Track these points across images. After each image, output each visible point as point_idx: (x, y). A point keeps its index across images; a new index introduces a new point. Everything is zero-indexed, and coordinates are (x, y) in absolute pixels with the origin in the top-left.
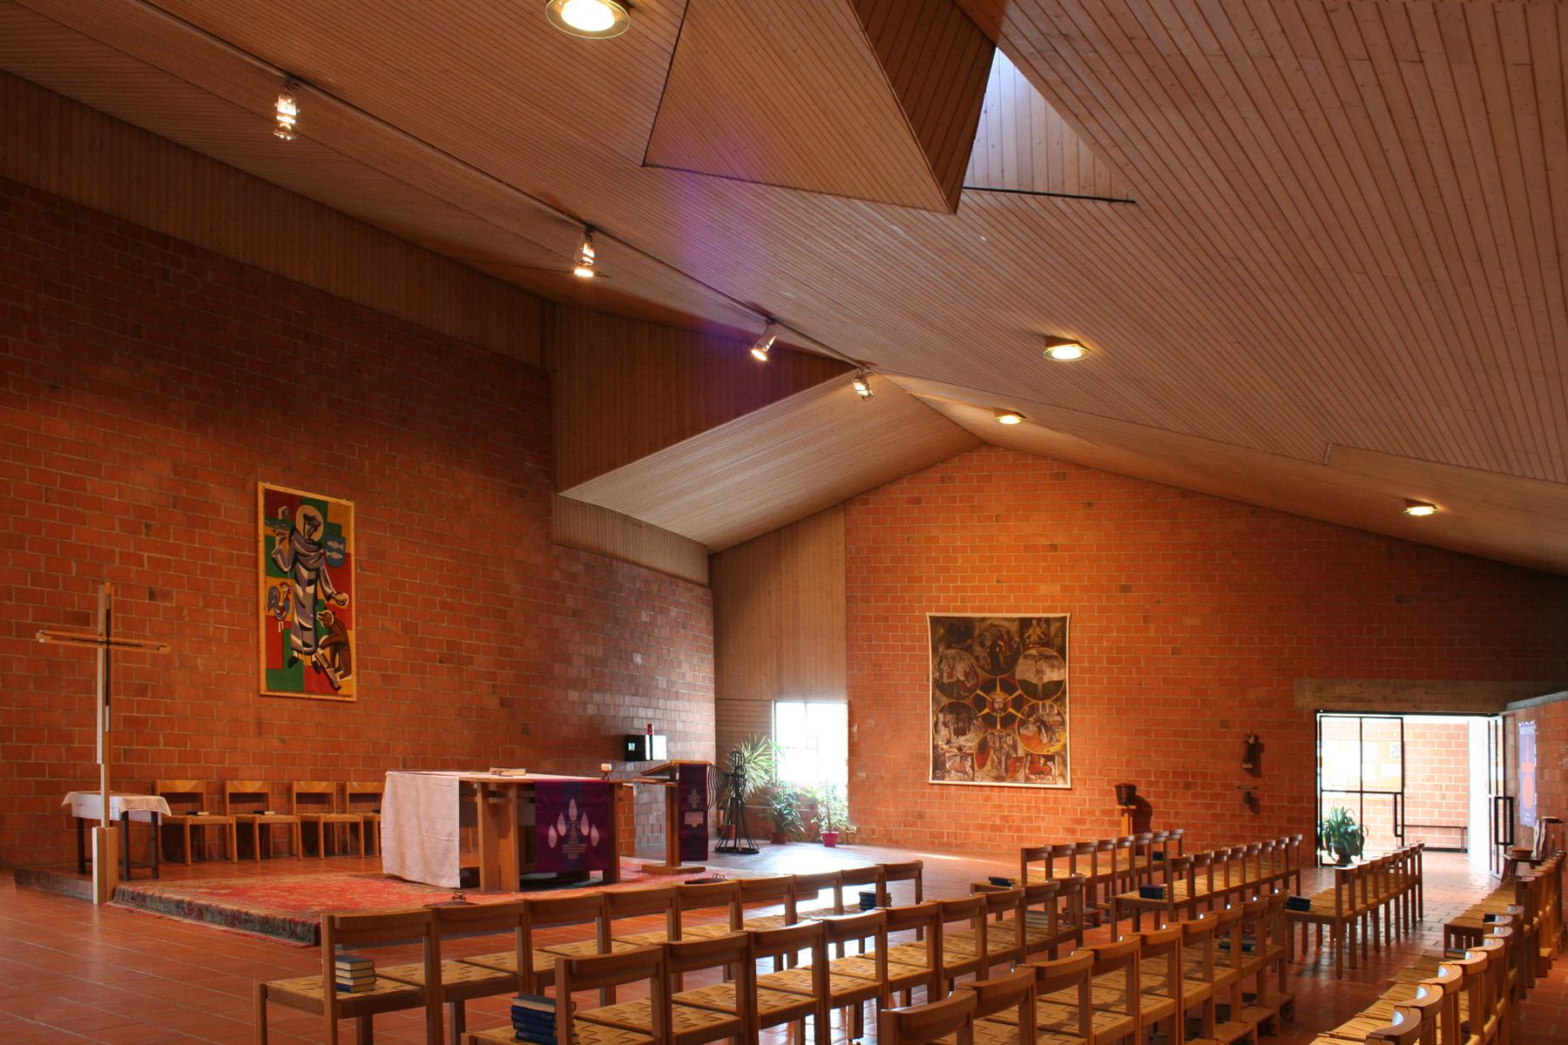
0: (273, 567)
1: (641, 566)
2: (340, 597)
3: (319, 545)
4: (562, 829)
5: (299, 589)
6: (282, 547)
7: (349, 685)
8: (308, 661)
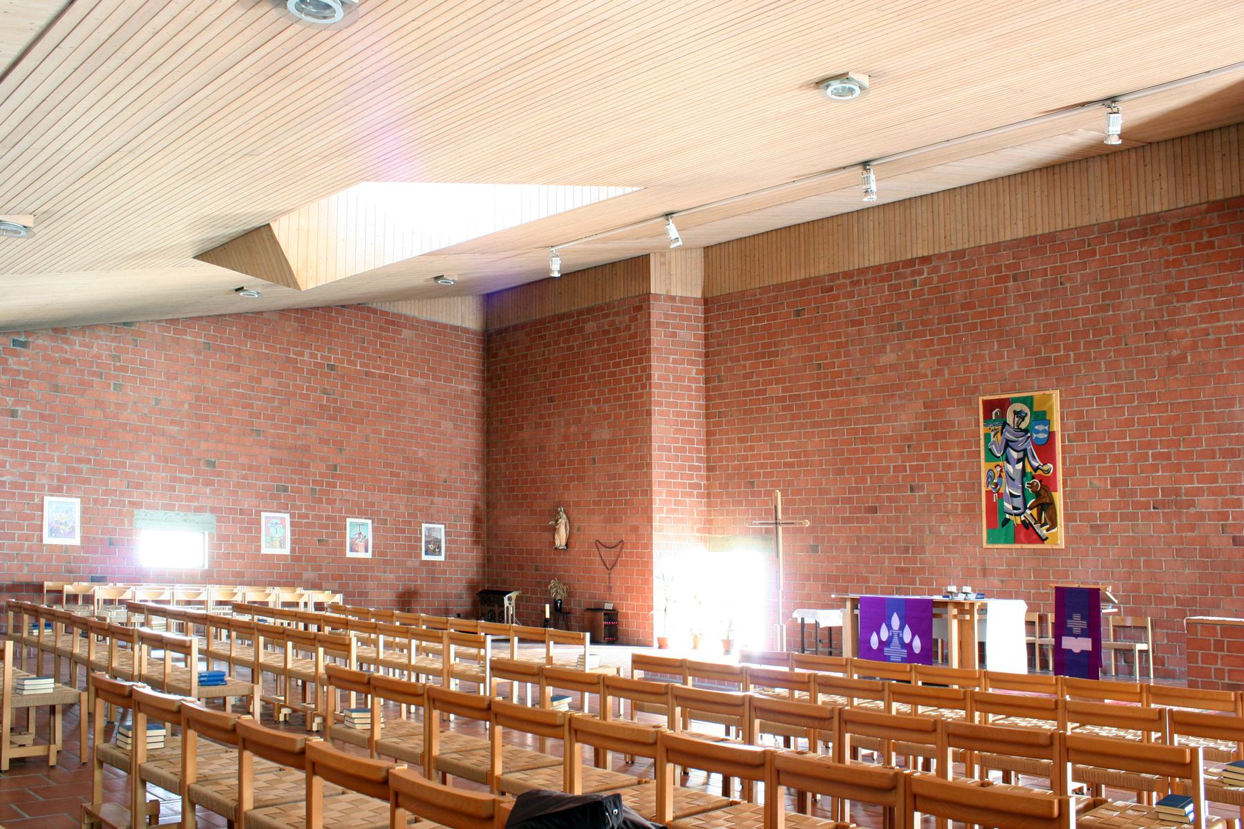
3: (1026, 431)
5: (1010, 468)
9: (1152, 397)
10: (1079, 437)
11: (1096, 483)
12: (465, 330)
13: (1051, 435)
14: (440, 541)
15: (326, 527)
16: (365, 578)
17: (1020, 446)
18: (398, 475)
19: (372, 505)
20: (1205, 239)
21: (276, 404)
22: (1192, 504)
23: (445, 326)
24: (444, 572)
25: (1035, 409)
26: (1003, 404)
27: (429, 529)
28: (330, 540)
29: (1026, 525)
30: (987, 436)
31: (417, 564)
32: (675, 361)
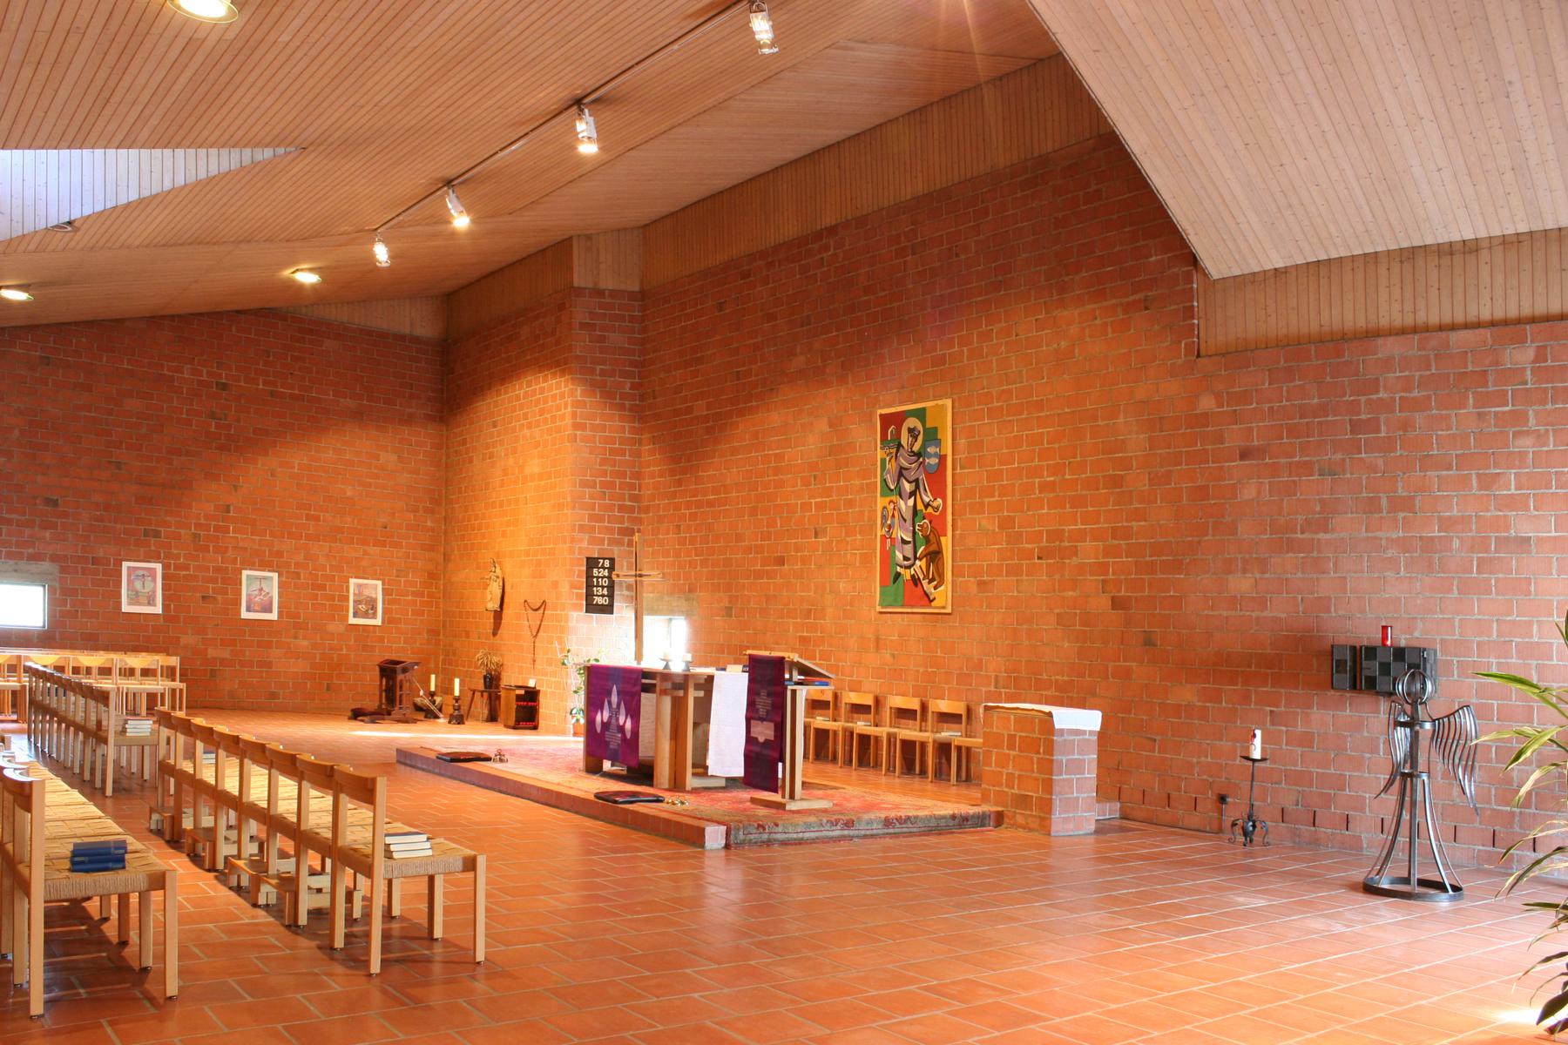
0: (886, 490)
1: (1453, 327)
2: (935, 504)
3: (918, 455)
4: (606, 715)
5: (902, 503)
6: (892, 466)
7: (943, 596)
8: (907, 574)
9: (1039, 405)
10: (970, 463)
11: (984, 523)
12: (416, 340)
13: (943, 458)
14: (375, 600)
15: (214, 581)
16: (269, 645)
17: (912, 475)
18: (317, 518)
19: (280, 554)
20: (1093, 187)
21: (144, 430)
22: (1074, 552)
23: (383, 335)
24: (381, 639)
25: (928, 426)
26: (898, 419)
27: (360, 586)
28: (220, 598)
29: (915, 581)
30: (883, 461)
31: (342, 628)
32: (603, 373)
